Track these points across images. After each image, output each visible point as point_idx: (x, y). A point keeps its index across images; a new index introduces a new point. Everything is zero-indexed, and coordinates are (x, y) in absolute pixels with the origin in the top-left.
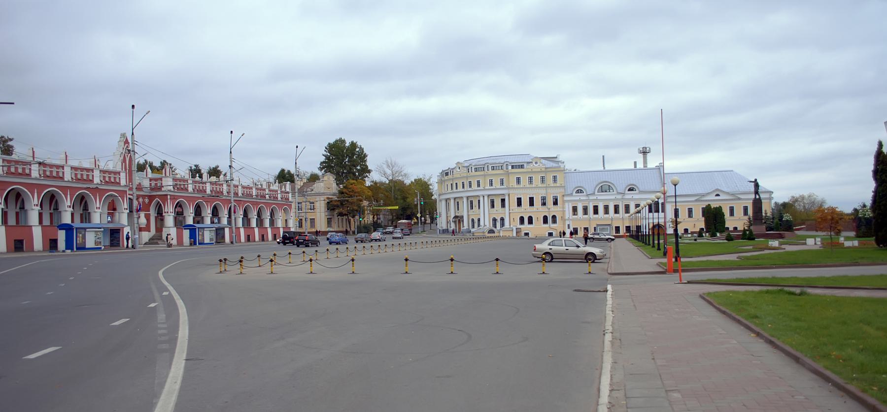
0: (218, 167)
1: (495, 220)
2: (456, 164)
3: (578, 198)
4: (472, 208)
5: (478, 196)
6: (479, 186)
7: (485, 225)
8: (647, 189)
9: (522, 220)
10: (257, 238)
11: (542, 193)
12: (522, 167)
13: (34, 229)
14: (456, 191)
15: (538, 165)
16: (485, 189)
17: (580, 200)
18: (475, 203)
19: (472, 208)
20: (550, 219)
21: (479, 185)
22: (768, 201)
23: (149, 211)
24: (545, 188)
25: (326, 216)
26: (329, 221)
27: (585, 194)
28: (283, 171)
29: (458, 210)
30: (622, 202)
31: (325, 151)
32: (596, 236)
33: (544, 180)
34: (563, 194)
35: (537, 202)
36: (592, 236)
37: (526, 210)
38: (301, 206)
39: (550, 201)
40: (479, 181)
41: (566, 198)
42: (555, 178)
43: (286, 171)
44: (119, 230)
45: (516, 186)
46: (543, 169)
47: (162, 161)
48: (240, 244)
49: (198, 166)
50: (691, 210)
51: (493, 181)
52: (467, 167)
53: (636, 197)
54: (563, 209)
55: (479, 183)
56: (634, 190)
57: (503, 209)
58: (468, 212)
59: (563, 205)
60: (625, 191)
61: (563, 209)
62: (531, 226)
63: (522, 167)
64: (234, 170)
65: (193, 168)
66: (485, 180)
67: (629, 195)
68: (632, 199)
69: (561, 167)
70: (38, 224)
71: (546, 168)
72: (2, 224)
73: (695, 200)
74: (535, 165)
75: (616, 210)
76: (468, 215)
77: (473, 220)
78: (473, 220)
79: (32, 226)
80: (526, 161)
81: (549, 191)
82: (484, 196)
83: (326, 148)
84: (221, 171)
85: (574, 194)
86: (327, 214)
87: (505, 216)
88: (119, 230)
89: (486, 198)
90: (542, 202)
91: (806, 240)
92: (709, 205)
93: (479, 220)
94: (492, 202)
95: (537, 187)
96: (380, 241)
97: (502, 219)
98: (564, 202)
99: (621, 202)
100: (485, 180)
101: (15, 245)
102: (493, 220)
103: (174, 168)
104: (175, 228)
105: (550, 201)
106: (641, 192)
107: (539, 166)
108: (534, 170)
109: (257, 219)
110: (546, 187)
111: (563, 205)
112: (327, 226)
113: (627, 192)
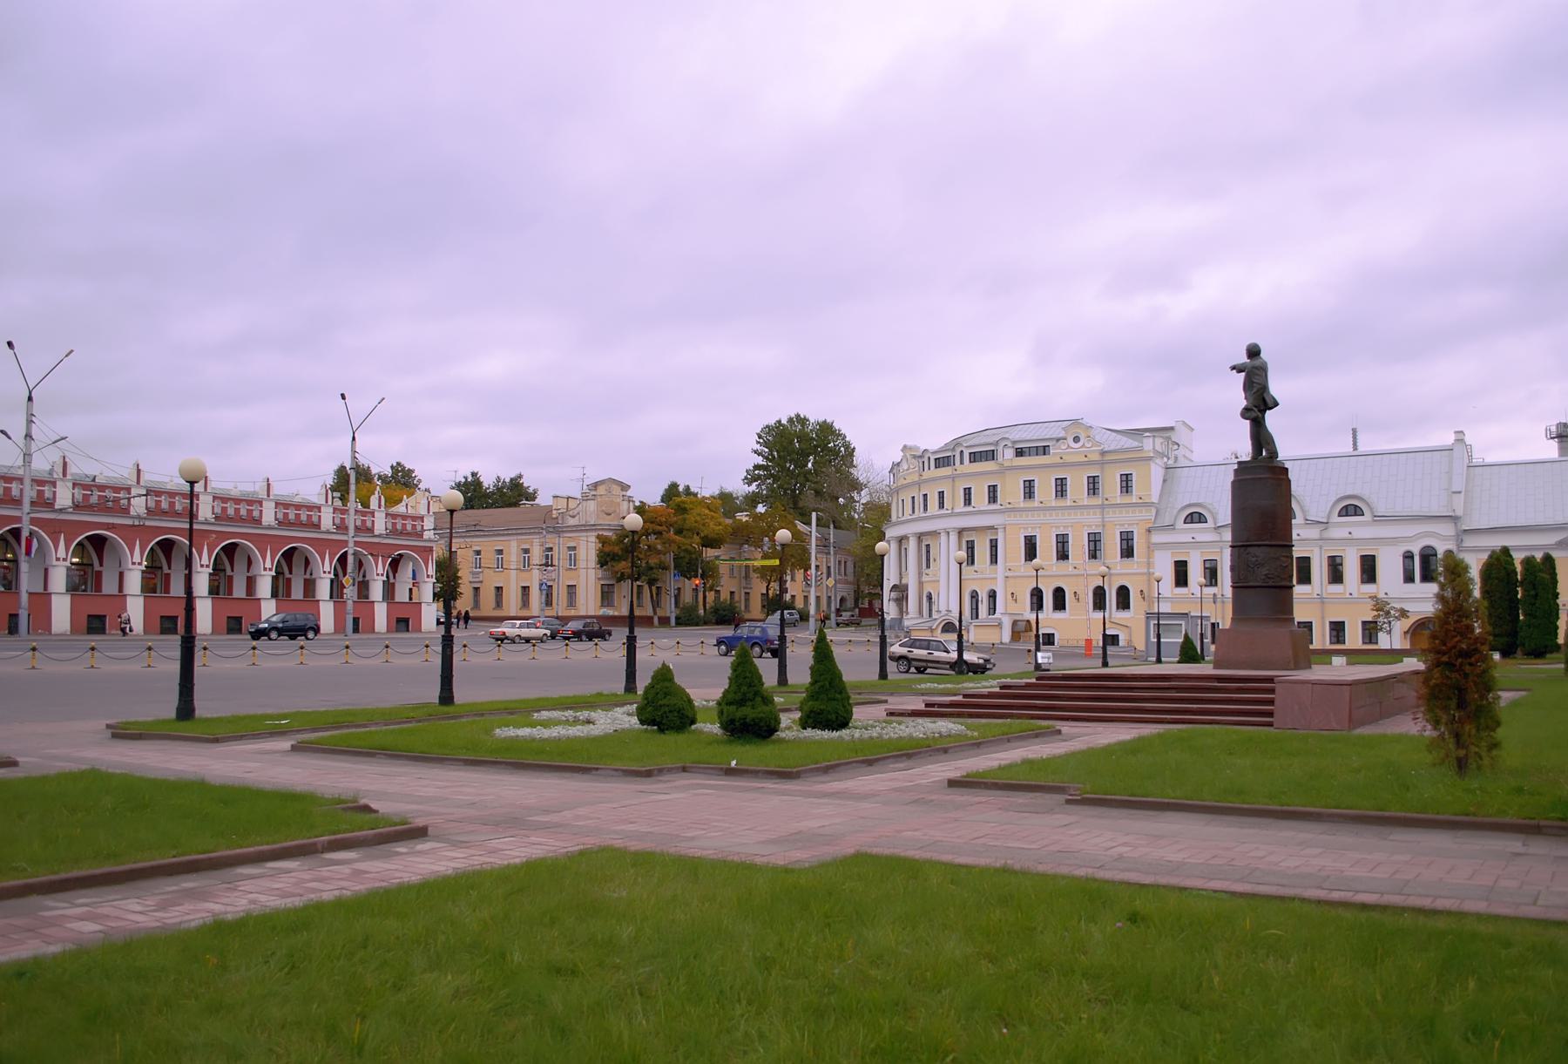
0: (520, 476)
3: (1187, 538)
4: (973, 563)
6: (970, 504)
8: (1400, 510)
9: (1037, 596)
10: (137, 622)
11: (1092, 522)
12: (1045, 450)
13: (263, 604)
14: (924, 515)
15: (1080, 444)
16: (953, 515)
17: (1195, 544)
18: (982, 552)
20: (1111, 598)
21: (970, 500)
24: (1098, 511)
25: (599, 579)
26: (606, 596)
27: (1210, 524)
28: (673, 487)
29: (928, 566)
30: (1321, 547)
31: (758, 442)
32: (916, 651)
34: (1151, 525)
35: (1079, 547)
36: (904, 651)
37: (1052, 574)
38: (552, 555)
39: (1112, 545)
40: (970, 488)
41: (1157, 538)
43: (681, 489)
45: (1022, 505)
46: (1096, 457)
47: (395, 464)
48: (49, 637)
49: (477, 474)
50: (1338, 561)
52: (920, 457)
53: (1359, 533)
54: (1149, 568)
55: (970, 494)
56: (1359, 512)
57: (993, 567)
58: (920, 574)
59: (1149, 558)
60: (1329, 517)
61: (1149, 568)
62: (1059, 615)
63: (1045, 450)
64: (34, 447)
65: (469, 480)
66: (953, 486)
67: (1343, 528)
68: (1350, 541)
69: (1146, 448)
70: (328, 598)
71: (1103, 453)
72: (383, 599)
73: (1556, 544)
74: (1073, 445)
75: (1336, 575)
76: (921, 584)
79: (259, 599)
80: (1054, 436)
81: (1111, 515)
82: (948, 533)
83: (760, 437)
84: (507, 476)
85: (1180, 524)
86: (600, 573)
90: (1125, 547)
92: (1506, 551)
95: (1076, 507)
96: (514, 642)
97: (993, 595)
98: (1151, 548)
99: (1317, 550)
100: (953, 486)
101: (88, 623)
102: (1032, 595)
103: (417, 479)
104: (385, 604)
105: (1112, 545)
106: (1379, 519)
107: (1083, 446)
108: (1068, 459)
109: (332, 581)
110: (1102, 507)
111: (1149, 558)
112: (600, 604)
113: (1335, 518)
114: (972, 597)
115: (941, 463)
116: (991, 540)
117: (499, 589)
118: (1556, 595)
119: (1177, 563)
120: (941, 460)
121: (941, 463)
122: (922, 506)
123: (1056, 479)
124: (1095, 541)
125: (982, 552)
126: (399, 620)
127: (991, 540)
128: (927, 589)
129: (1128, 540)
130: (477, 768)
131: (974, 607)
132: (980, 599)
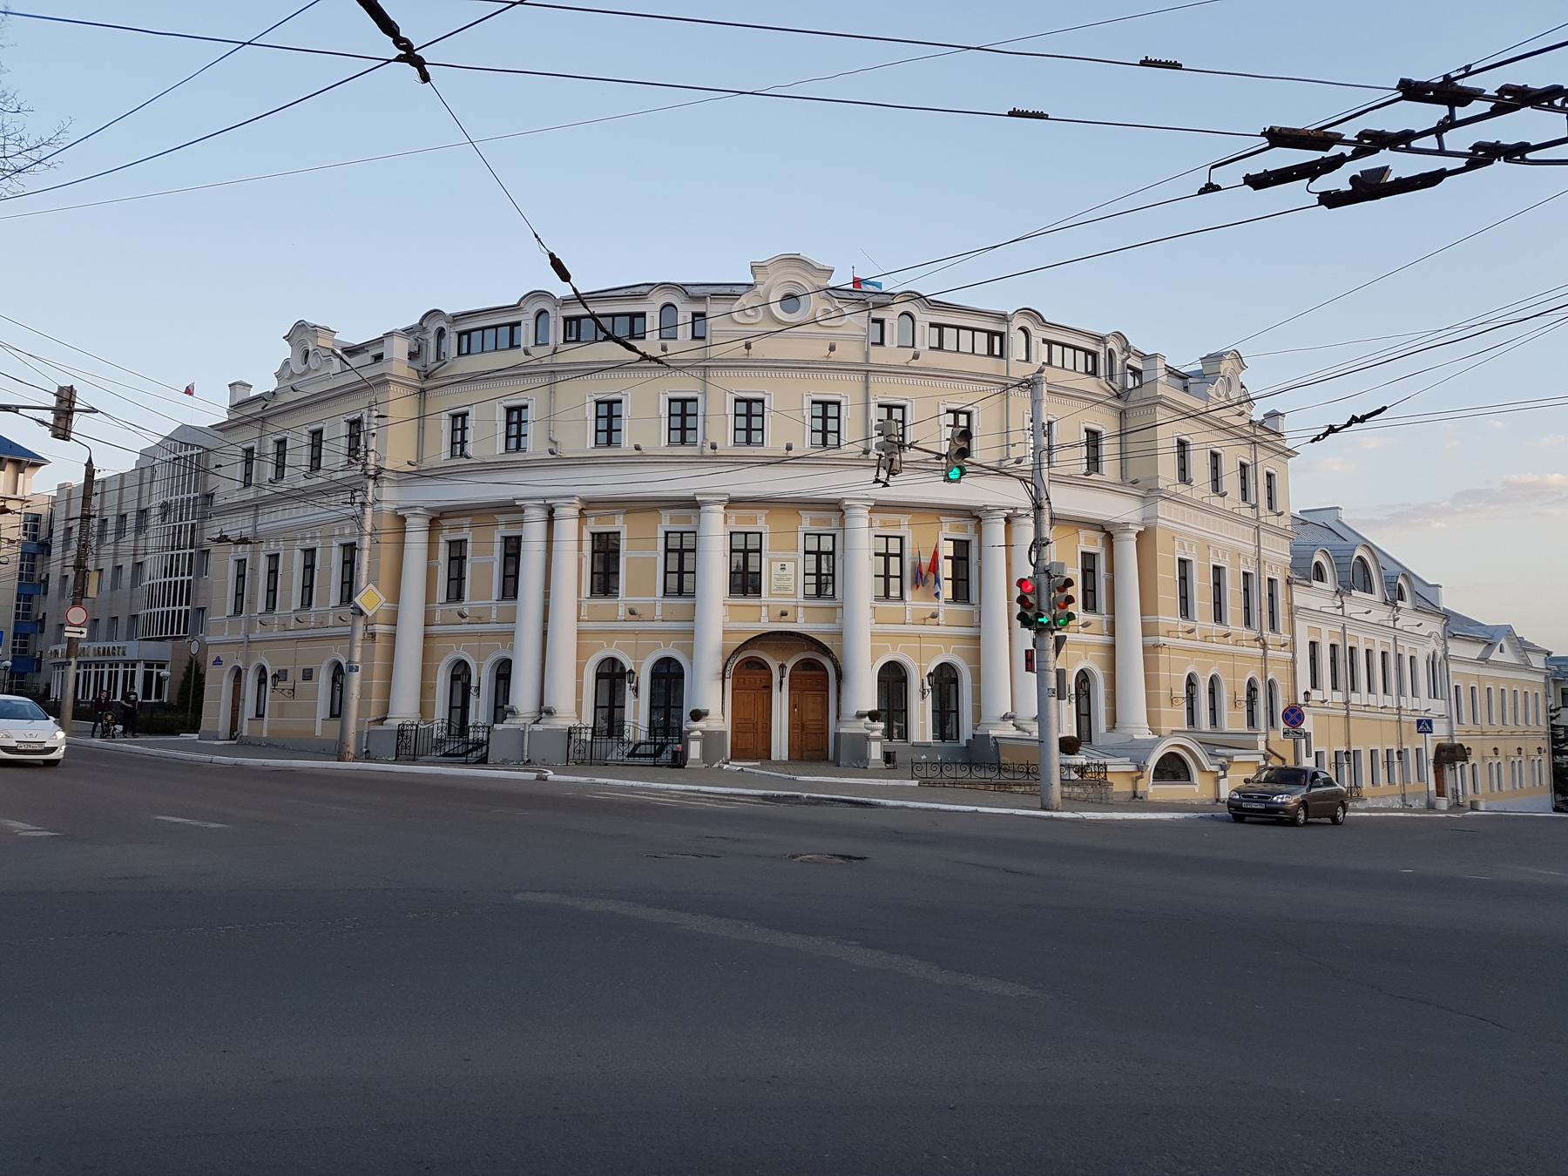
1: (612, 676)
2: (1264, 415)
4: (459, 597)
5: (512, 509)
7: (544, 711)
18: (484, 563)
19: (456, 592)
22: (824, 557)
23: (145, 672)
33: (756, 423)
42: (749, 415)
44: (1189, 780)
51: (626, 410)
77: (460, 672)
78: (460, 672)
87: (690, 656)
88: (1189, 780)
89: (567, 528)
91: (974, 735)
93: (503, 672)
94: (605, 553)
102: (599, 676)
114: (454, 678)
115: (490, 344)
116: (507, 539)
117: (1351, 649)
118: (1446, 131)
119: (1311, 643)
120: (476, 336)
121: (490, 344)
122: (1266, 613)
123: (671, 401)
124: (681, 552)
125: (484, 563)
126: (310, 678)
127: (507, 539)
128: (1399, 651)
129: (681, 552)
130: (1372, 664)
131: (458, 702)
132: (474, 683)
